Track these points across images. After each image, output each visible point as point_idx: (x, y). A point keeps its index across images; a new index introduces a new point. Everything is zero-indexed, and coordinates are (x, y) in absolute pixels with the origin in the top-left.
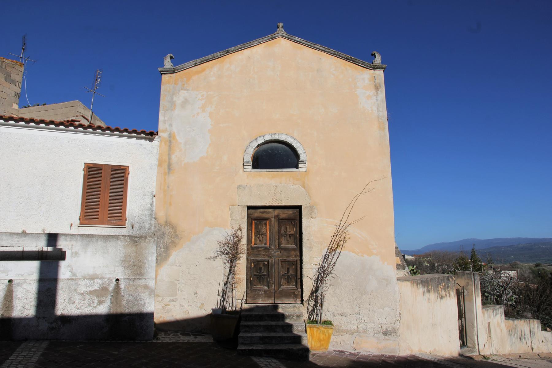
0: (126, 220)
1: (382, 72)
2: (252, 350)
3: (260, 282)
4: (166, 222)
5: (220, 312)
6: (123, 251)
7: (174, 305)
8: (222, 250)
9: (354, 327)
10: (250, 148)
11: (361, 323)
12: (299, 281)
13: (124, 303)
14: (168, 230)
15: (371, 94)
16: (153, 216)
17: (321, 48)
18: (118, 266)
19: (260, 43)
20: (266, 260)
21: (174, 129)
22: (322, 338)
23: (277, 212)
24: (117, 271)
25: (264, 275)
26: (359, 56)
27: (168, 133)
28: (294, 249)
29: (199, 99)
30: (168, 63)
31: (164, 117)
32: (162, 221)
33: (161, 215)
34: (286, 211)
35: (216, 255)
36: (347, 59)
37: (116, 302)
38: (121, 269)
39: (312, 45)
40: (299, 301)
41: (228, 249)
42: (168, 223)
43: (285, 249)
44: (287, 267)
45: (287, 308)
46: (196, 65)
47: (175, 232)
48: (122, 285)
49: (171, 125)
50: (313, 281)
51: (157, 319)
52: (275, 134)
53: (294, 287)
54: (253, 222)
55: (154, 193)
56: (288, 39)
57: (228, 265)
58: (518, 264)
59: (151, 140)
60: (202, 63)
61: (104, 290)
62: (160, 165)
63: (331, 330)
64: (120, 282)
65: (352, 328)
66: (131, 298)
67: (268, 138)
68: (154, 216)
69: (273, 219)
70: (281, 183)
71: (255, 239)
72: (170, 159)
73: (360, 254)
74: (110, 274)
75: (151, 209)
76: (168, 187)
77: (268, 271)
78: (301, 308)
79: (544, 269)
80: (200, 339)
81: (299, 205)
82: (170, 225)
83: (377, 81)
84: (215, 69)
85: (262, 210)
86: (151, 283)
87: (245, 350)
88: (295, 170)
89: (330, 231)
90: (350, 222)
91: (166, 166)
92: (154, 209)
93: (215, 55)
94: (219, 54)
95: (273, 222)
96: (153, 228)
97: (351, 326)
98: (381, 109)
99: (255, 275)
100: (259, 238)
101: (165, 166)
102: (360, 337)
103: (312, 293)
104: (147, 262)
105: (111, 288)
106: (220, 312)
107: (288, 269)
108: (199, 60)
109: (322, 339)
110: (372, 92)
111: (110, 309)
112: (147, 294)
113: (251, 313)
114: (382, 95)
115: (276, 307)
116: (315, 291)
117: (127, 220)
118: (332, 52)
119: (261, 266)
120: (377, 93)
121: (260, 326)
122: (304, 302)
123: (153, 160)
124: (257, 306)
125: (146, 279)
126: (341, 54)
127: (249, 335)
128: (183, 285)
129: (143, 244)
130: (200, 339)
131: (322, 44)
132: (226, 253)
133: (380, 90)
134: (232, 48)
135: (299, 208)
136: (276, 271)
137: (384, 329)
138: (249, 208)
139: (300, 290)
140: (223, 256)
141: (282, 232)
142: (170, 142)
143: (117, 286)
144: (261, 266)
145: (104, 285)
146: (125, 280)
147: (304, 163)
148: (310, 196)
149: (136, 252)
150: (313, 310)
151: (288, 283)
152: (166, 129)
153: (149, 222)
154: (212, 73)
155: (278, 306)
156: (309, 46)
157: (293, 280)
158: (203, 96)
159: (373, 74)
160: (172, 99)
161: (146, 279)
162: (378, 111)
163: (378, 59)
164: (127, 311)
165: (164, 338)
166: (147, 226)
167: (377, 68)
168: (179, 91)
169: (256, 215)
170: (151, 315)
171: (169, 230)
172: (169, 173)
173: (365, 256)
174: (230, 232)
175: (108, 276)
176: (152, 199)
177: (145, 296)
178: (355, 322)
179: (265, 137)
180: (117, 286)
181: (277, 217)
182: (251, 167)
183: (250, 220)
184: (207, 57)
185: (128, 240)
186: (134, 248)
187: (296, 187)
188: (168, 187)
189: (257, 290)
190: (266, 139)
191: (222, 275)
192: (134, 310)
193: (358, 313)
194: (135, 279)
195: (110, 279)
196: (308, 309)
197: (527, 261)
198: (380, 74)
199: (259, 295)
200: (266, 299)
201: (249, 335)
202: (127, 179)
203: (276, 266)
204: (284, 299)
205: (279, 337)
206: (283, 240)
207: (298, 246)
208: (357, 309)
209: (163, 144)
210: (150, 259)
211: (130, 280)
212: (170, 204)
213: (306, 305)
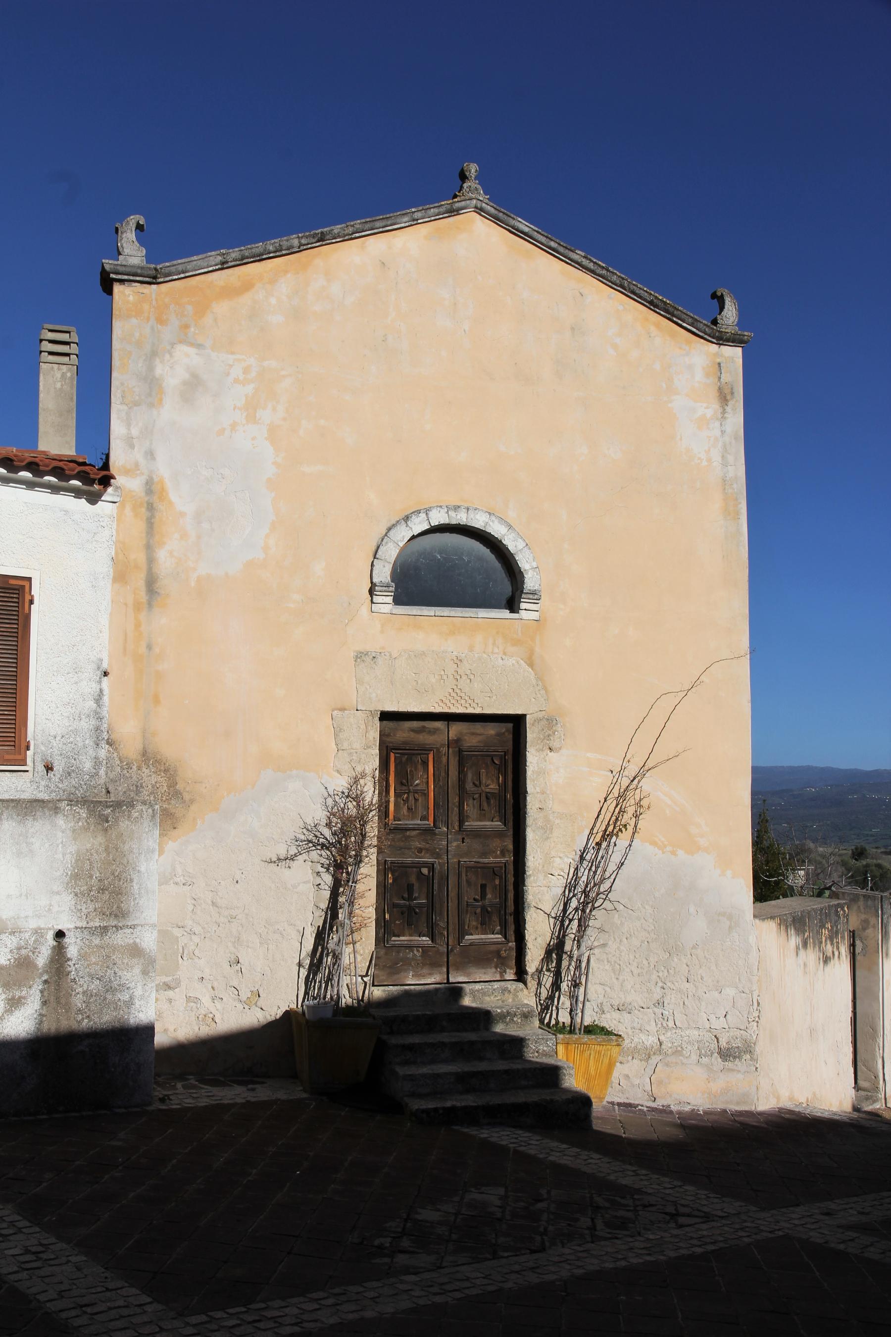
0: (28, 748)
1: (739, 351)
2: (453, 1109)
3: (409, 924)
4: (144, 753)
5: (329, 1014)
6: (72, 848)
7: (170, 1001)
8: (311, 837)
9: (651, 1041)
10: (391, 545)
11: (666, 1029)
12: (511, 919)
13: (78, 1001)
14: (149, 777)
15: (709, 413)
16: (105, 737)
17: (585, 262)
18: (58, 893)
19: (414, 222)
20: (425, 864)
21: (163, 470)
22: (592, 1071)
23: (456, 729)
24: (55, 909)
25: (420, 906)
26: (687, 305)
27: (144, 478)
28: (500, 834)
29: (236, 381)
30: (132, 252)
31: (129, 425)
32: (131, 749)
33: (128, 731)
34: (478, 727)
35: (293, 850)
36: (652, 305)
37: (58, 999)
38: (67, 900)
39: (561, 249)
40: (510, 974)
41: (327, 832)
42: (148, 757)
43: (477, 834)
44: (480, 882)
45: (484, 994)
46: (224, 266)
47: (172, 784)
48: (72, 951)
49: (150, 455)
50: (552, 920)
51: (161, 1039)
52: (456, 508)
53: (498, 937)
54: (392, 755)
55: (105, 666)
56: (496, 220)
57: (328, 879)
58: (810, 851)
59: (94, 498)
60: (242, 261)
61: (24, 964)
62: (120, 576)
63: (615, 1050)
64: (66, 940)
65: (648, 1044)
66: (95, 986)
67: (439, 518)
68: (105, 736)
69: (444, 750)
70: (471, 649)
71: (396, 805)
72: (151, 561)
73: (669, 848)
74: (39, 917)
75: (96, 713)
76: (149, 647)
77: (431, 896)
78: (520, 994)
79: (879, 866)
80: (263, 1093)
81: (520, 712)
82: (157, 762)
83: (725, 378)
84: (284, 287)
85: (415, 724)
86: (148, 940)
87: (436, 1110)
88: (506, 613)
89: (594, 787)
90: (651, 766)
91: (143, 583)
92: (105, 713)
93: (285, 244)
94: (296, 242)
95: (444, 759)
96: (102, 772)
97: (643, 1037)
98: (730, 458)
99: (395, 906)
100: (406, 801)
101: (139, 580)
102: (667, 1065)
103: (548, 953)
104: (135, 877)
105: (42, 959)
106: (329, 1014)
107: (483, 887)
108: (234, 253)
109: (593, 1072)
110: (709, 408)
111: (41, 1022)
112: (137, 970)
113: (392, 1013)
114: (736, 419)
115: (456, 992)
116: (555, 950)
117: (32, 747)
118: (614, 278)
119: (413, 879)
120: (724, 412)
121: (443, 1044)
122: (529, 978)
123: (99, 560)
124: (407, 994)
125: (133, 927)
126: (642, 289)
127: (425, 1070)
128: (196, 939)
129: (124, 824)
130: (263, 1093)
131: (590, 252)
132: (323, 845)
133: (731, 403)
134: (337, 229)
135: (517, 722)
136: (453, 894)
137: (723, 1043)
138: (385, 716)
139: (512, 944)
140: (314, 855)
141: (469, 786)
142: (151, 507)
143: (59, 951)
144: (413, 879)
145: (23, 952)
146: (78, 934)
147: (535, 595)
148: (545, 688)
149: (107, 849)
150: (551, 998)
151: (485, 925)
152: (137, 465)
153: (91, 752)
154: (273, 301)
155: (461, 989)
156: (553, 252)
157: (495, 918)
158: (246, 370)
159: (717, 355)
160: (151, 368)
161: (133, 927)
162: (725, 464)
163: (730, 314)
164: (85, 1024)
165: (187, 1096)
166: (88, 766)
167: (728, 340)
168: (173, 345)
169: (405, 740)
170: (148, 1030)
171: (154, 779)
172: (150, 605)
173: (681, 853)
174: (341, 783)
175: (33, 924)
176: (100, 682)
177: (131, 976)
178: (652, 1027)
179: (431, 514)
180: (59, 951)
181: (455, 743)
182: (390, 599)
183: (387, 749)
184: (259, 247)
185: (84, 813)
186: (100, 839)
187: (510, 662)
188: (149, 647)
189: (400, 946)
190: (435, 523)
191: (311, 907)
192: (104, 1019)
193: (660, 1003)
194: (104, 930)
195: (38, 932)
196: (538, 995)
197: (824, 841)
198: (734, 354)
199: (407, 963)
200: (425, 971)
201: (425, 1070)
202: (28, 617)
203: (452, 880)
204: (472, 970)
205: (506, 1072)
206: (470, 808)
207: (511, 824)
208: (657, 994)
209: (128, 511)
210: (143, 869)
211: (92, 931)
212: (157, 700)
213: (532, 983)
